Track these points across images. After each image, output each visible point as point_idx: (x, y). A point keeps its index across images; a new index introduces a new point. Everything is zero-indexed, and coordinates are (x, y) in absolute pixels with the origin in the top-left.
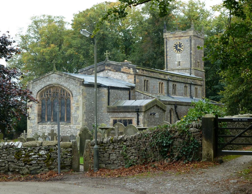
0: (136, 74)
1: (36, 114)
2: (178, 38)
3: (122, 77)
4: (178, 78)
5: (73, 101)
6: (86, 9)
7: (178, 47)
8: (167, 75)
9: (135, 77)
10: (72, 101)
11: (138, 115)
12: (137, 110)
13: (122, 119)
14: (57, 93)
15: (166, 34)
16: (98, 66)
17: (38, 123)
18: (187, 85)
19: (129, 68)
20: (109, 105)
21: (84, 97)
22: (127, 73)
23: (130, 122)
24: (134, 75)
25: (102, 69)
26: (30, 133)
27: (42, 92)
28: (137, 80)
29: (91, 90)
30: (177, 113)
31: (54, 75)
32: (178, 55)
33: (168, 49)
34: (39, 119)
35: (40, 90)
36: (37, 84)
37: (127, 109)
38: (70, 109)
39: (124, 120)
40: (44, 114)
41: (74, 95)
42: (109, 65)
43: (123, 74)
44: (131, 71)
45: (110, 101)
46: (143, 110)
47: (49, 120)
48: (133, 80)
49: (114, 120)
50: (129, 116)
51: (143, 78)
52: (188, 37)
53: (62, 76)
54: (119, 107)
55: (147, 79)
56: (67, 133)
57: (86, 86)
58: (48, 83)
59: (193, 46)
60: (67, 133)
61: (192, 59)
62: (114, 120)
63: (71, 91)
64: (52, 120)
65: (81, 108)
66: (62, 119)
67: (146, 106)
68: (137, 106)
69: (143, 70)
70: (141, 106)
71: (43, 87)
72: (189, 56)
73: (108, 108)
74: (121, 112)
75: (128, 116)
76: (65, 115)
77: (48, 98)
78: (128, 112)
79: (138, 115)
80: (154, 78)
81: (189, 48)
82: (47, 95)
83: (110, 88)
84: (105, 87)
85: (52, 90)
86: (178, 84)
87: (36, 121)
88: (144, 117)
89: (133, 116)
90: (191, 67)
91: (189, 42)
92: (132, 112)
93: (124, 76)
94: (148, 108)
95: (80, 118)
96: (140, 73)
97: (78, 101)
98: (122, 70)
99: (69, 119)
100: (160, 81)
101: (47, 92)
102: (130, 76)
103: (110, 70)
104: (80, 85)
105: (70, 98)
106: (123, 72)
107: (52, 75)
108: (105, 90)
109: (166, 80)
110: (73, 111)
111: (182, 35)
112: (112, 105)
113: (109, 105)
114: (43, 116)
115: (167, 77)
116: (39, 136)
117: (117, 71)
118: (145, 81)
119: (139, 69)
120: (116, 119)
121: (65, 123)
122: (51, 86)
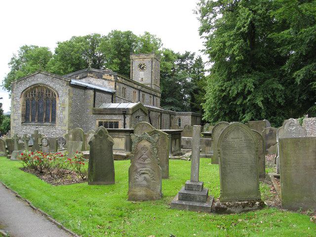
0: (116, 81)
1: (20, 115)
2: (141, 60)
3: (103, 83)
4: (146, 90)
5: (58, 102)
6: (71, 37)
7: (141, 67)
8: (139, 85)
9: (115, 84)
10: (58, 102)
11: (125, 118)
12: (124, 112)
13: (108, 121)
14: (42, 93)
15: (132, 56)
16: (26, 201)
17: (22, 123)
18: (152, 96)
19: (111, 75)
20: (94, 107)
21: (70, 98)
22: (108, 80)
23: (117, 124)
24: (114, 83)
25: (85, 75)
26: (12, 131)
27: (27, 92)
28: (117, 87)
29: (77, 91)
30: (150, 118)
31: (40, 74)
32: (142, 73)
33: (133, 68)
34: (22, 119)
35: (25, 90)
36: (21, 84)
37: (113, 112)
38: (56, 110)
39: (110, 122)
40: (29, 114)
41: (60, 95)
42: (91, 72)
43: (104, 80)
44: (112, 78)
45: (96, 104)
46: (131, 112)
47: (33, 120)
48: (114, 86)
49: (99, 122)
50: (115, 119)
51: (122, 86)
52: (150, 59)
53: (48, 75)
54: (105, 109)
55: (125, 86)
56: (52, 134)
57: (72, 87)
58: (33, 83)
59: (154, 66)
60: (52, 134)
61: (153, 76)
62: (99, 122)
63: (57, 91)
64: (36, 121)
65: (67, 108)
66: (47, 120)
67: (133, 109)
68: (124, 109)
69: (122, 78)
70: (127, 109)
71: (27, 87)
72: (150, 74)
73: (94, 110)
74: (107, 114)
75: (115, 118)
76: (51, 116)
77: (33, 98)
78: (115, 114)
79: (125, 118)
80: (132, 87)
81: (151, 67)
82: (32, 95)
83: (95, 90)
84: (91, 89)
85: (37, 90)
86: (146, 94)
87: (20, 121)
88: (131, 119)
89: (119, 119)
90: (152, 82)
91: (150, 63)
92: (119, 114)
93: (106, 83)
94: (135, 110)
95: (66, 119)
96: (120, 81)
97: (64, 102)
98: (104, 77)
99: (54, 120)
100: (134, 90)
101: (32, 93)
102: (111, 83)
103: (92, 77)
104: (67, 85)
105: (55, 99)
106: (104, 79)
107: (37, 75)
108: (92, 92)
109: (138, 90)
110: (58, 112)
111: (145, 57)
112: (97, 107)
113: (94, 107)
114: (27, 117)
115: (139, 87)
116: (20, 138)
117: (98, 78)
118: (123, 88)
119: (119, 77)
120: (102, 121)
121: (50, 124)
122: (36, 86)
